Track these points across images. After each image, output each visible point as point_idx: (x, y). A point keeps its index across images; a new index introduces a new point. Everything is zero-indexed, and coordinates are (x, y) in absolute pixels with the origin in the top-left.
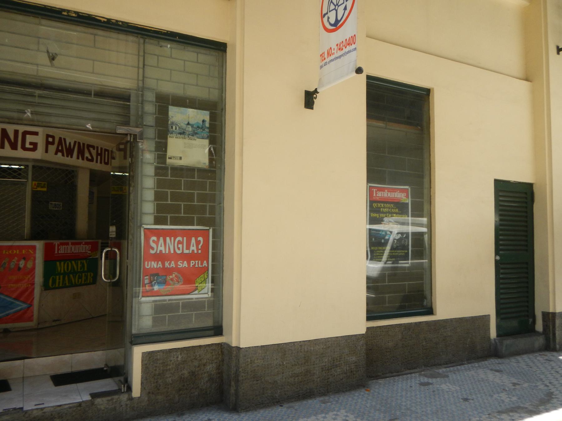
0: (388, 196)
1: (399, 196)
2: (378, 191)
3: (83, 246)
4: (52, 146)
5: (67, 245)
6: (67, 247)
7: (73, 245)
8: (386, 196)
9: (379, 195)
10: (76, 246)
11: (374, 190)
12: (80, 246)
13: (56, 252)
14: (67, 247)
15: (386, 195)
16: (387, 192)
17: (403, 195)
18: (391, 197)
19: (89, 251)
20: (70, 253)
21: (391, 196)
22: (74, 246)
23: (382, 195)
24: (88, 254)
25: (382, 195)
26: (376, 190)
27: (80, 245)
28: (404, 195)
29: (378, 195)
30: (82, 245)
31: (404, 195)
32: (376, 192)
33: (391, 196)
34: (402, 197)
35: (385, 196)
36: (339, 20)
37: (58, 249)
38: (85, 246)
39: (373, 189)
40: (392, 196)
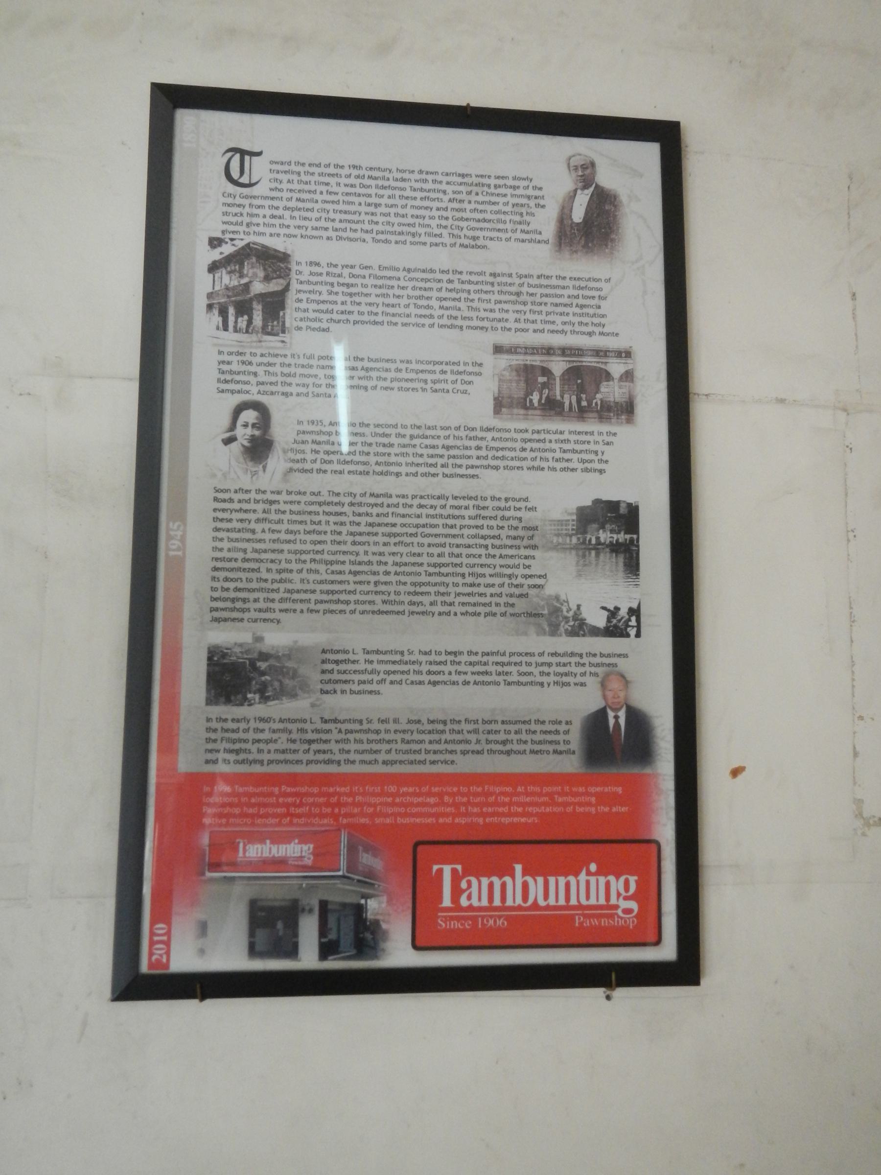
0: (531, 901)
1: (597, 898)
2: (467, 872)
3: (593, 880)
4: (580, 505)
5: (501, 877)
6: (504, 886)
7: (533, 876)
8: (519, 901)
9: (475, 902)
10: (552, 880)
11: (447, 870)
12: (572, 879)
13: (447, 902)
14: (504, 886)
15: (514, 898)
16: (524, 874)
17: (617, 885)
18: (548, 908)
19: (626, 898)
20: (520, 908)
21: (546, 896)
22: (540, 880)
23: (491, 898)
24: (619, 912)
25: (491, 898)
26: (459, 867)
27: (576, 874)
28: (627, 889)
29: (469, 897)
30: (583, 877)
31: (627, 889)
32: (456, 878)
33: (546, 896)
34: (613, 901)
35: (509, 902)
36: (564, 394)
37: (457, 892)
38: (602, 880)
39: (435, 867)
40: (552, 901)
